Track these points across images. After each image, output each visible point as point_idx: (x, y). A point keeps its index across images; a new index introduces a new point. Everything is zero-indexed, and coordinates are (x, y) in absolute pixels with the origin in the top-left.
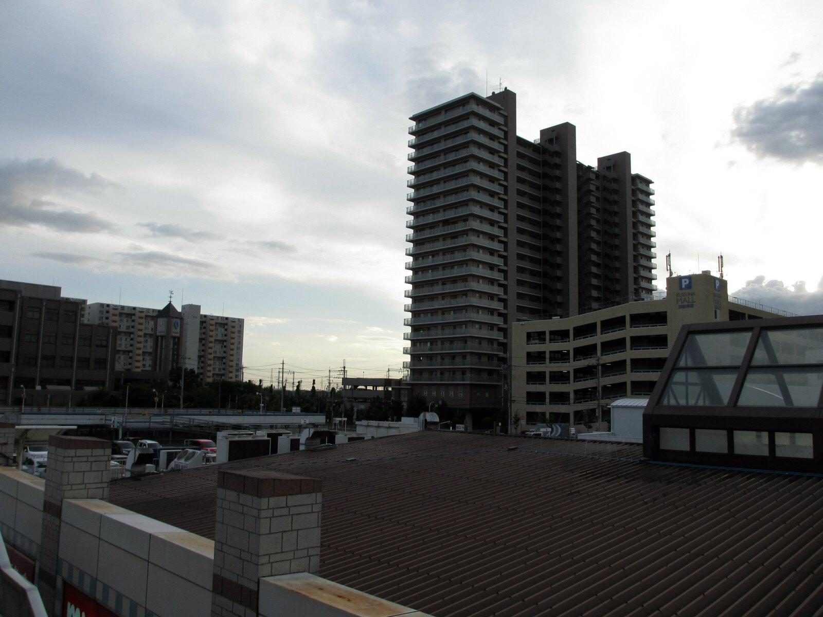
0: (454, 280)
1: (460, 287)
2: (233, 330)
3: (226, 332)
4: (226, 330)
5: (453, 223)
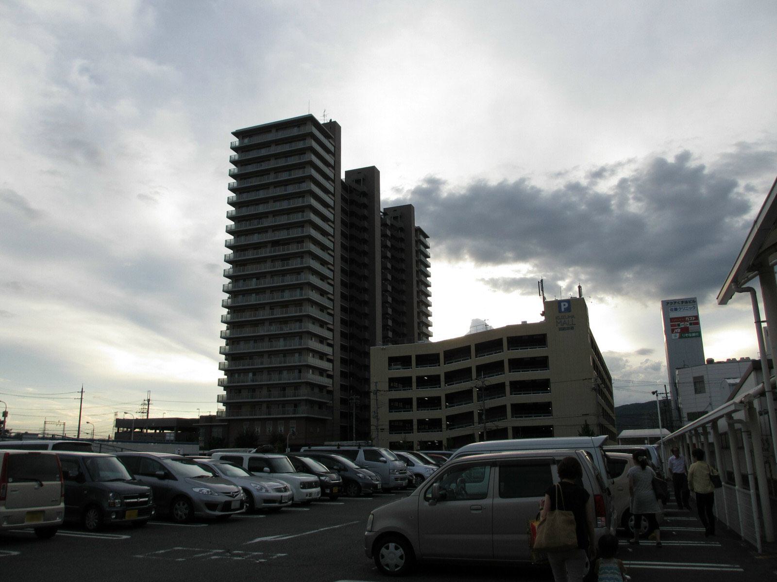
0: (285, 305)
1: (292, 312)
5: (284, 244)
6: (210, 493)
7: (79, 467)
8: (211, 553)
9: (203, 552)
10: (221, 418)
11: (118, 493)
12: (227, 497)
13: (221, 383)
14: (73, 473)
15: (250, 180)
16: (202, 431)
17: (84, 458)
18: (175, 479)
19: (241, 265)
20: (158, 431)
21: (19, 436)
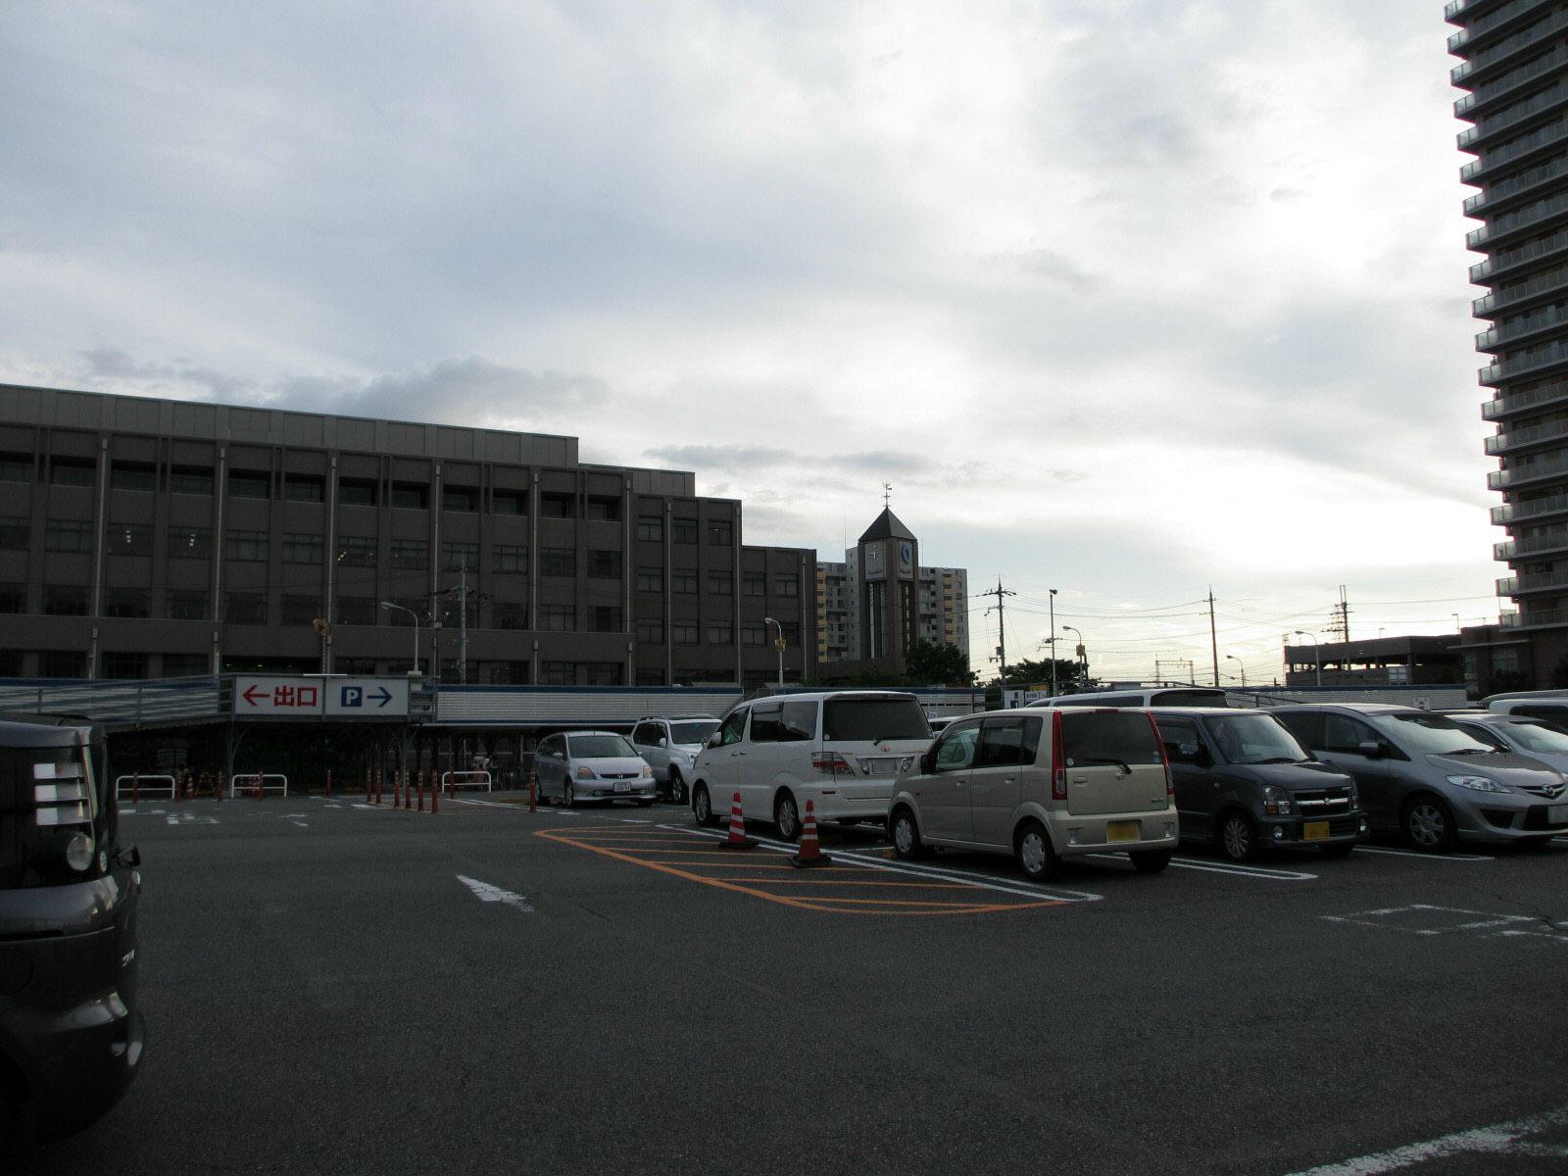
2: (947, 592)
3: (933, 599)
4: (933, 594)
6: (1490, 788)
7: (1199, 736)
8: (1503, 923)
9: (1483, 919)
10: (1509, 630)
11: (1281, 788)
12: (1535, 796)
13: (1500, 554)
14: (1189, 747)
15: (1505, 79)
16: (1469, 659)
17: (1205, 717)
18: (1403, 757)
19: (1510, 248)
20: (1373, 666)
21: (1114, 686)
